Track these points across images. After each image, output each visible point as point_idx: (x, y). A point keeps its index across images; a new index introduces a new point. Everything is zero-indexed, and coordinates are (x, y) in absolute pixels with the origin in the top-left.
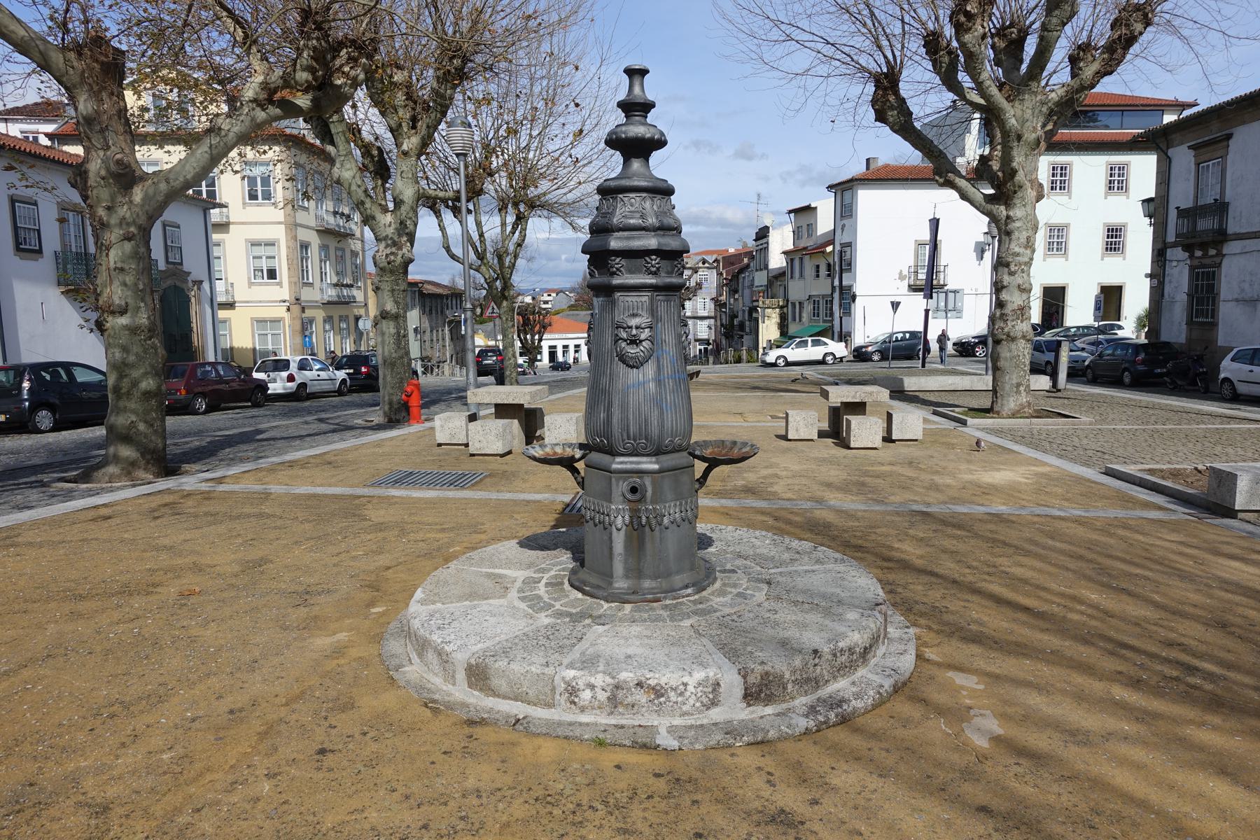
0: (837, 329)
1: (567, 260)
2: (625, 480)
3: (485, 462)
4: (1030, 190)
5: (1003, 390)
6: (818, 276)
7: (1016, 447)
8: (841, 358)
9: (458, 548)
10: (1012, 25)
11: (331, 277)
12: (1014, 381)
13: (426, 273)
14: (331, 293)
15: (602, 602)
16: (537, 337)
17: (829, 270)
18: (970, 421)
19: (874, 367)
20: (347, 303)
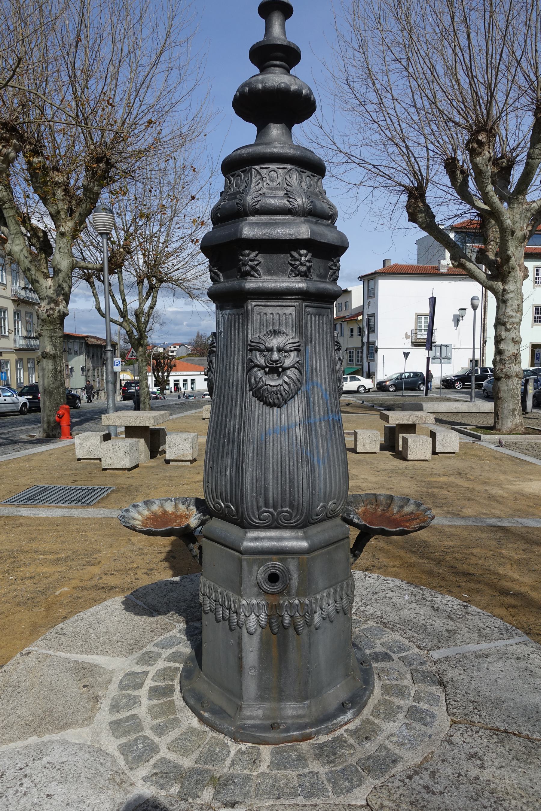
0: (365, 369)
1: (187, 325)
2: (261, 563)
3: (115, 476)
4: (519, 271)
5: (503, 413)
6: (352, 335)
7: (528, 459)
8: (369, 389)
9: (66, 589)
10: (502, 157)
11: (22, 332)
12: (511, 408)
13: (93, 333)
14: (22, 343)
15: (228, 741)
16: (166, 374)
17: (360, 332)
18: (483, 437)
19: (393, 396)
20: (34, 350)
